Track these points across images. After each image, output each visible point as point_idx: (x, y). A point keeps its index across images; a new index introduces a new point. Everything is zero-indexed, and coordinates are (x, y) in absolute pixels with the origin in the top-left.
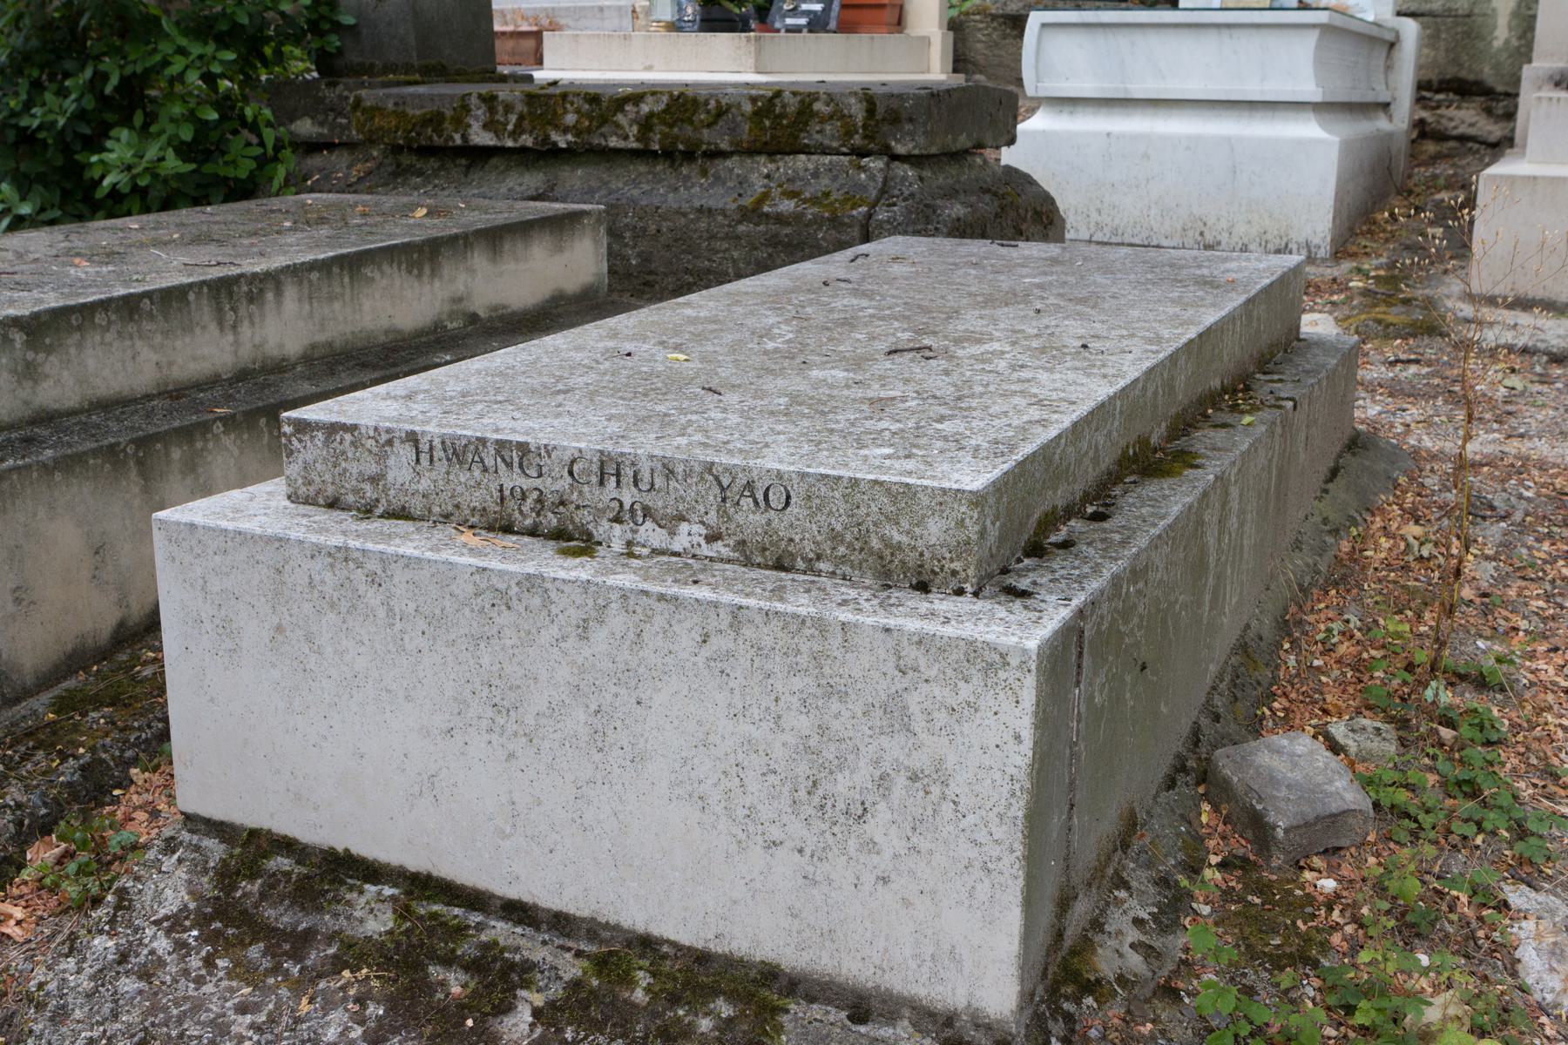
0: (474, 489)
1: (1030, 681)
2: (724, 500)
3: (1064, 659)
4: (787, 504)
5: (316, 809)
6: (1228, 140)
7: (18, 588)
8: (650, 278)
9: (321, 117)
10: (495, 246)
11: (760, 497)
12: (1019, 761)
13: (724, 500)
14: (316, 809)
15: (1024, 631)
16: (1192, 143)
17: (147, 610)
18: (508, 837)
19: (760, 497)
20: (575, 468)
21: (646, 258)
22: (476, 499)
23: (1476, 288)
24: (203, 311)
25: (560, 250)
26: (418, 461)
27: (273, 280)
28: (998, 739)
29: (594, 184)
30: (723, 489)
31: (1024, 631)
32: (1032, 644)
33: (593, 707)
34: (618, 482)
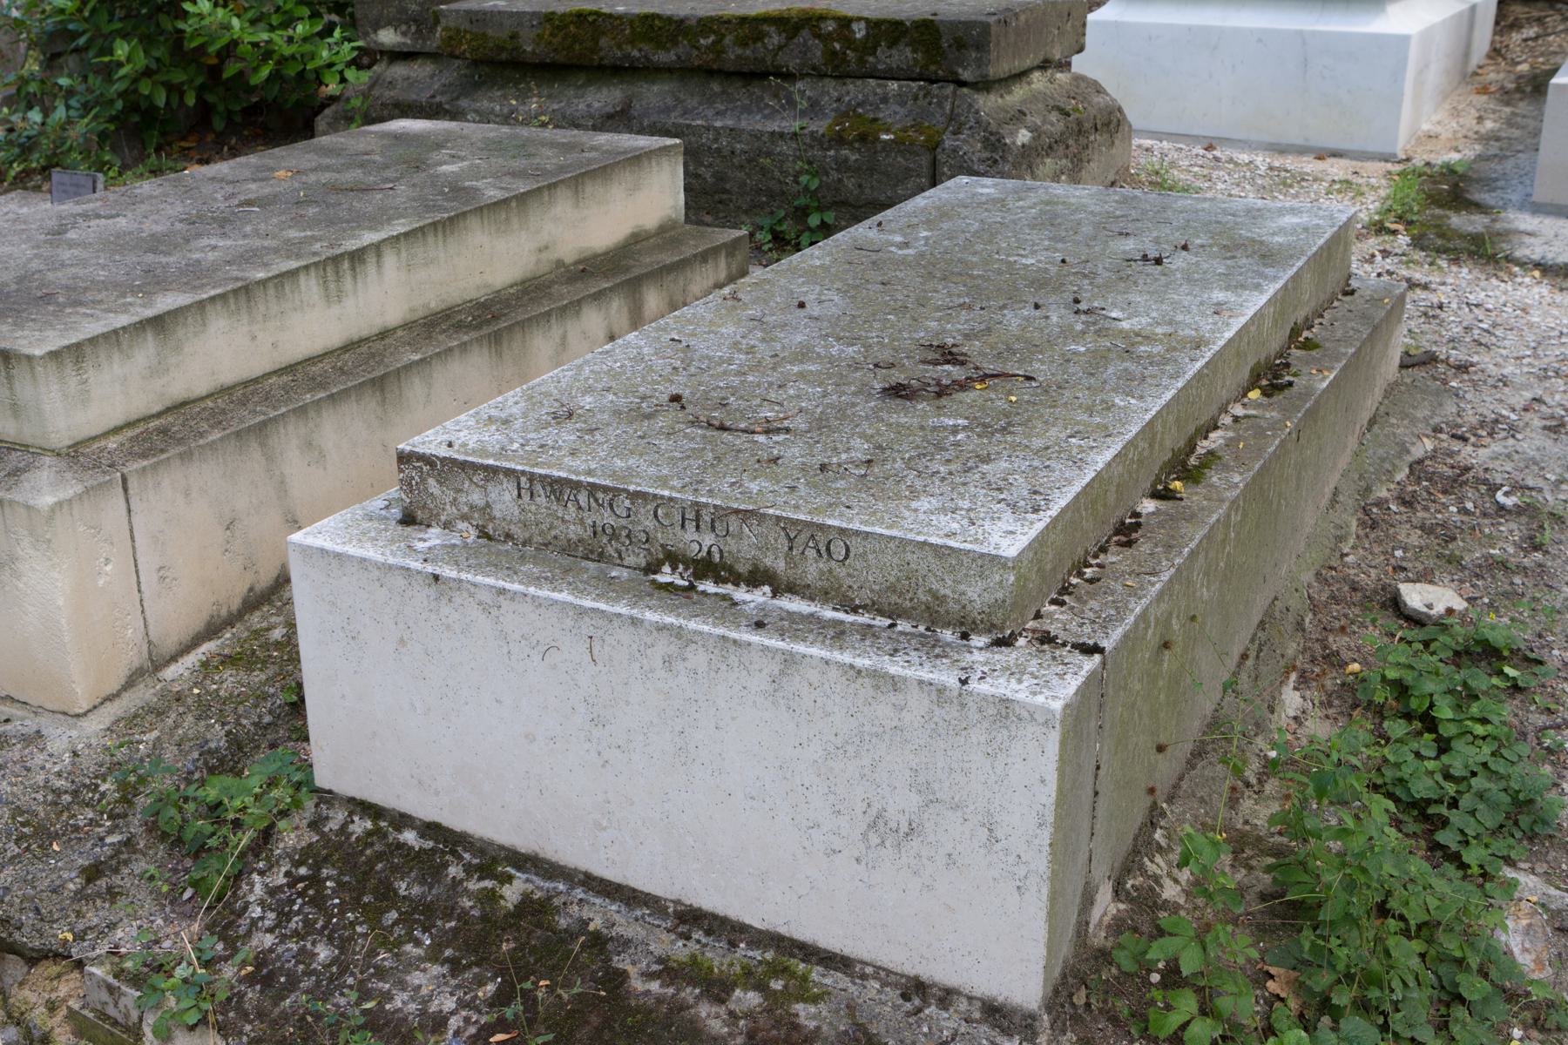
0: (572, 523)
1: (1054, 738)
2: (791, 549)
3: (1081, 720)
4: (847, 556)
5: (437, 793)
6: (1300, 33)
7: (161, 568)
8: (725, 196)
9: (404, 28)
10: (577, 192)
11: (823, 550)
12: (1044, 800)
13: (791, 549)
14: (437, 793)
15: (1054, 688)
16: (1262, 37)
17: (278, 564)
18: (605, 829)
19: (823, 550)
20: (660, 512)
21: (720, 178)
22: (574, 531)
23: (1535, 198)
24: (310, 286)
25: (636, 188)
26: (519, 496)
27: (377, 248)
28: (1028, 778)
29: (669, 101)
30: (790, 540)
31: (1054, 688)
32: (1057, 706)
33: (679, 728)
34: (698, 527)
